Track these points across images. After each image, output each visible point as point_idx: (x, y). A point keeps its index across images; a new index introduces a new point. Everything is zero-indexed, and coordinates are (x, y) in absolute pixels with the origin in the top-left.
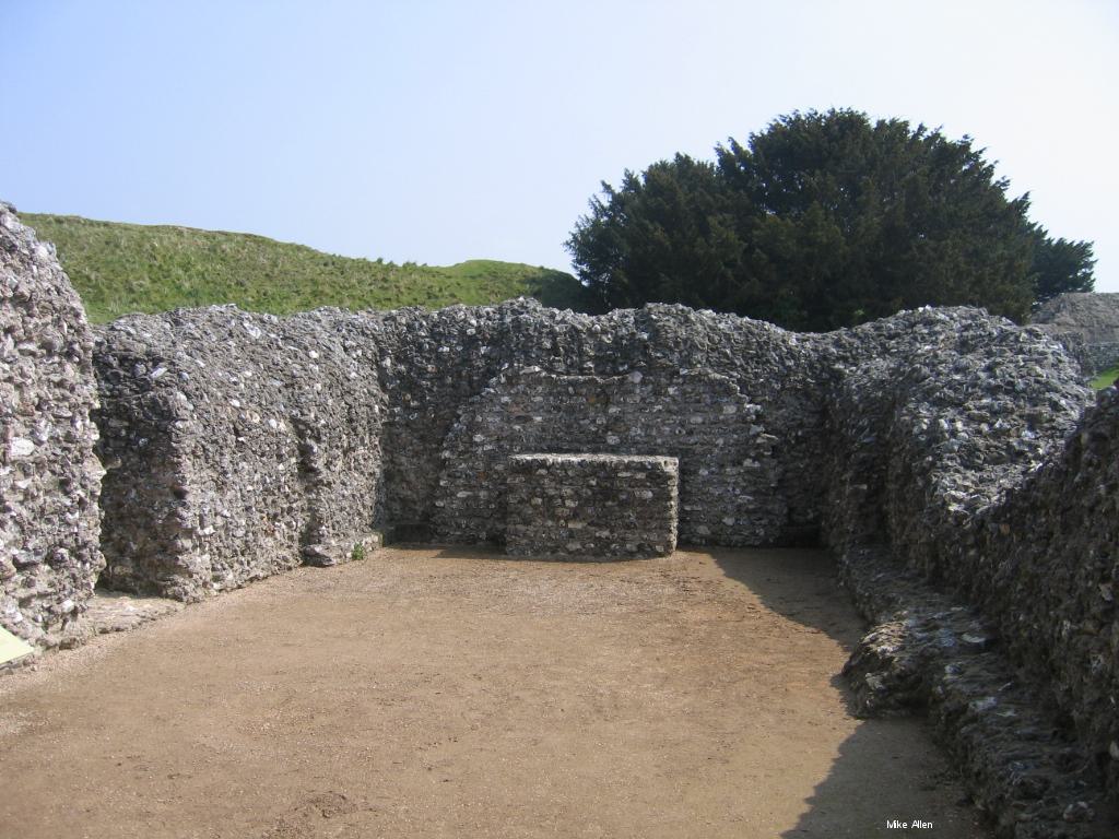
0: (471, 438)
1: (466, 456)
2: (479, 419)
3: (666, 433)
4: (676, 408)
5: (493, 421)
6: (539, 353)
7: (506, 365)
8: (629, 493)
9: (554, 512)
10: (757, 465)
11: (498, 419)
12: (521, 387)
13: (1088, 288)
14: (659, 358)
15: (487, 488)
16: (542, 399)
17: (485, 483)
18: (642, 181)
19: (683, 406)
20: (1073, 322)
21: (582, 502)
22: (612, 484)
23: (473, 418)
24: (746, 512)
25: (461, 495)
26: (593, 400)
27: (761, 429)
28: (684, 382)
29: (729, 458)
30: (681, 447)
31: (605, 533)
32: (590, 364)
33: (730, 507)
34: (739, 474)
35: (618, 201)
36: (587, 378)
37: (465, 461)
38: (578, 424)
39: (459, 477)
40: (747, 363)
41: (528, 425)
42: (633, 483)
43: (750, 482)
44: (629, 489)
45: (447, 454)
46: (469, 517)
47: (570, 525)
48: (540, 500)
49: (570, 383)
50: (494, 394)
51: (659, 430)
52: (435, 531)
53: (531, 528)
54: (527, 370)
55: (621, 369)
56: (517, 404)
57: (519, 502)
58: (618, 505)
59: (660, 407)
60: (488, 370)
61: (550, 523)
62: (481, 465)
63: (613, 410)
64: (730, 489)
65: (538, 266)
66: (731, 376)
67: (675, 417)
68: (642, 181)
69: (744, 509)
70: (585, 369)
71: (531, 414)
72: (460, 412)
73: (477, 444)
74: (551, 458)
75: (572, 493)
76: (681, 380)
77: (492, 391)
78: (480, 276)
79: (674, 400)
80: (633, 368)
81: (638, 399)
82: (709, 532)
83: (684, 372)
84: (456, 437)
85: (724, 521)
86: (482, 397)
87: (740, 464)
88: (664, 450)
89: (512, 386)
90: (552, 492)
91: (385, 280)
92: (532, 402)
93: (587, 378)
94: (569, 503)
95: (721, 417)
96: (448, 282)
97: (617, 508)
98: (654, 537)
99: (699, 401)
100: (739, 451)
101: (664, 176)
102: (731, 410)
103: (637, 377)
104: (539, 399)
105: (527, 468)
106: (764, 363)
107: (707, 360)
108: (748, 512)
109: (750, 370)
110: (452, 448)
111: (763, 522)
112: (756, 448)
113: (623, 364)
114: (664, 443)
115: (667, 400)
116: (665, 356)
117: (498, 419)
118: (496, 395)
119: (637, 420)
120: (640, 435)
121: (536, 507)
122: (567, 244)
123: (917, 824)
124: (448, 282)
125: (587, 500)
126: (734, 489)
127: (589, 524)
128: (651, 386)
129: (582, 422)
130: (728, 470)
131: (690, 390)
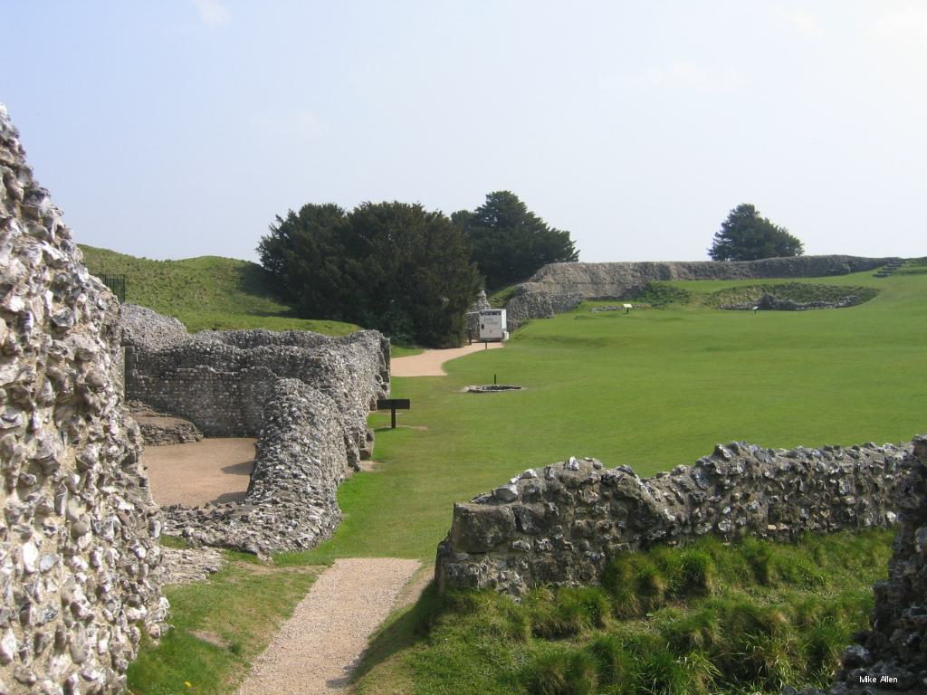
13: (577, 260)
18: (298, 215)
20: (552, 281)
35: (285, 227)
65: (241, 259)
68: (298, 215)
78: (210, 268)
91: (161, 274)
96: (194, 273)
101: (372, 218)
122: (257, 249)
123: (885, 679)
124: (194, 273)
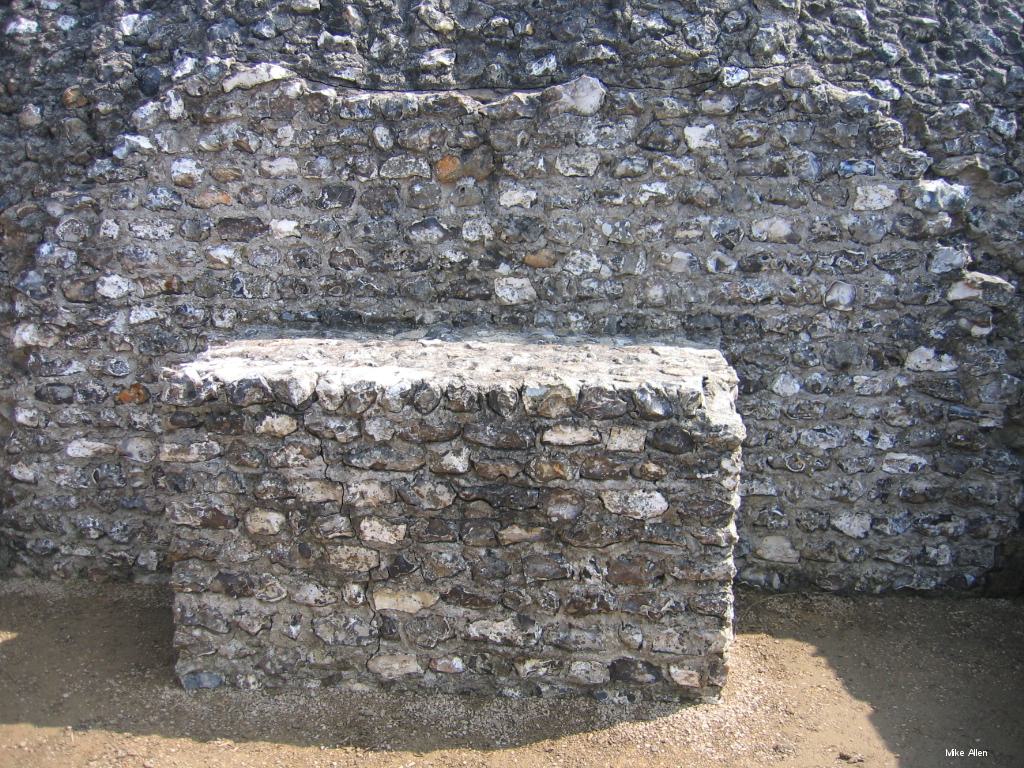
0: (92, 284)
1: (82, 340)
2: (111, 229)
3: (677, 269)
4: (709, 191)
5: (153, 235)
6: (286, 23)
7: (189, 64)
8: (582, 497)
9: (324, 557)
10: (947, 364)
11: (164, 230)
12: (230, 131)
14: (656, 34)
15: (148, 432)
16: (293, 166)
17: (141, 418)
19: (729, 183)
21: (420, 526)
22: (524, 469)
23: (95, 227)
24: (905, 500)
25: (80, 448)
26: (451, 166)
27: (960, 257)
28: (737, 109)
29: (866, 343)
30: (721, 310)
31: (501, 628)
32: (440, 56)
33: (858, 486)
34: (894, 390)
36: (429, 97)
37: (82, 353)
38: (407, 240)
39: (70, 401)
40: (916, 56)
41: (254, 244)
42: (601, 464)
43: (921, 414)
44: (585, 484)
45: (25, 335)
46: (109, 508)
47: (383, 602)
48: (275, 520)
49: (382, 115)
50: (150, 154)
51: (653, 256)
52: (20, 544)
53: (251, 605)
54: (246, 77)
55: (536, 70)
56: (221, 182)
57: (206, 524)
58: (545, 539)
59: (661, 188)
60: (140, 83)
61: (312, 592)
62: (126, 366)
63: (513, 197)
64: (864, 435)
66: (875, 92)
67: (704, 220)
69: (897, 491)
70: (427, 70)
71: (263, 212)
72: (56, 210)
73: (110, 305)
74: (315, 365)
75: (384, 496)
76: (726, 104)
77: (144, 143)
79: (703, 167)
80: (572, 66)
81: (590, 162)
82: (793, 555)
83: (734, 77)
84: (49, 280)
85: (837, 523)
86: (117, 163)
87: (898, 361)
88: (672, 321)
89: (205, 125)
90: (315, 493)
92: (266, 175)
93: (429, 97)
94: (372, 529)
95: (848, 221)
97: (538, 548)
98: (665, 640)
99: (779, 171)
100: (896, 323)
102: (877, 196)
103: (588, 94)
104: (284, 165)
105: (225, 412)
106: (963, 56)
107: (801, 39)
108: (910, 499)
109: (925, 77)
110: (43, 317)
111: (950, 527)
112: (948, 316)
113: (539, 56)
114: (668, 299)
115: (685, 165)
116: (673, 27)
117: (164, 230)
118: (156, 155)
119: (587, 227)
120: (595, 275)
121: (261, 540)
123: (973, 752)
125: (437, 526)
126: (874, 436)
127: (443, 597)
128: (631, 122)
129: (417, 236)
130: (860, 379)
131: (754, 135)
